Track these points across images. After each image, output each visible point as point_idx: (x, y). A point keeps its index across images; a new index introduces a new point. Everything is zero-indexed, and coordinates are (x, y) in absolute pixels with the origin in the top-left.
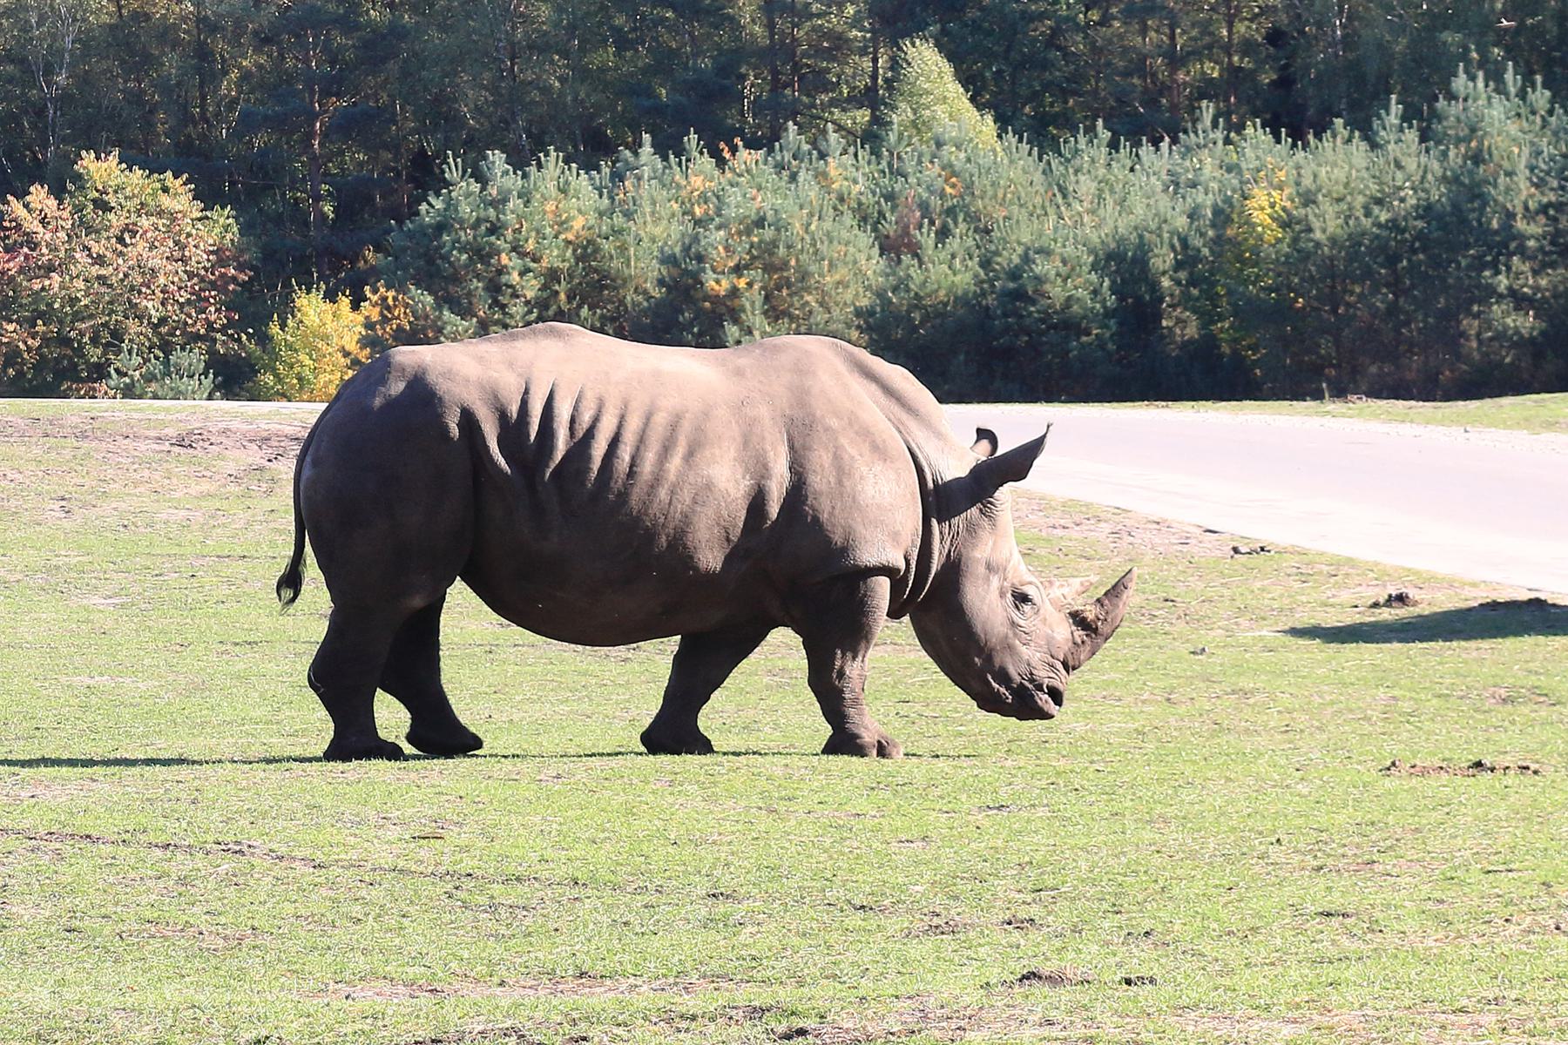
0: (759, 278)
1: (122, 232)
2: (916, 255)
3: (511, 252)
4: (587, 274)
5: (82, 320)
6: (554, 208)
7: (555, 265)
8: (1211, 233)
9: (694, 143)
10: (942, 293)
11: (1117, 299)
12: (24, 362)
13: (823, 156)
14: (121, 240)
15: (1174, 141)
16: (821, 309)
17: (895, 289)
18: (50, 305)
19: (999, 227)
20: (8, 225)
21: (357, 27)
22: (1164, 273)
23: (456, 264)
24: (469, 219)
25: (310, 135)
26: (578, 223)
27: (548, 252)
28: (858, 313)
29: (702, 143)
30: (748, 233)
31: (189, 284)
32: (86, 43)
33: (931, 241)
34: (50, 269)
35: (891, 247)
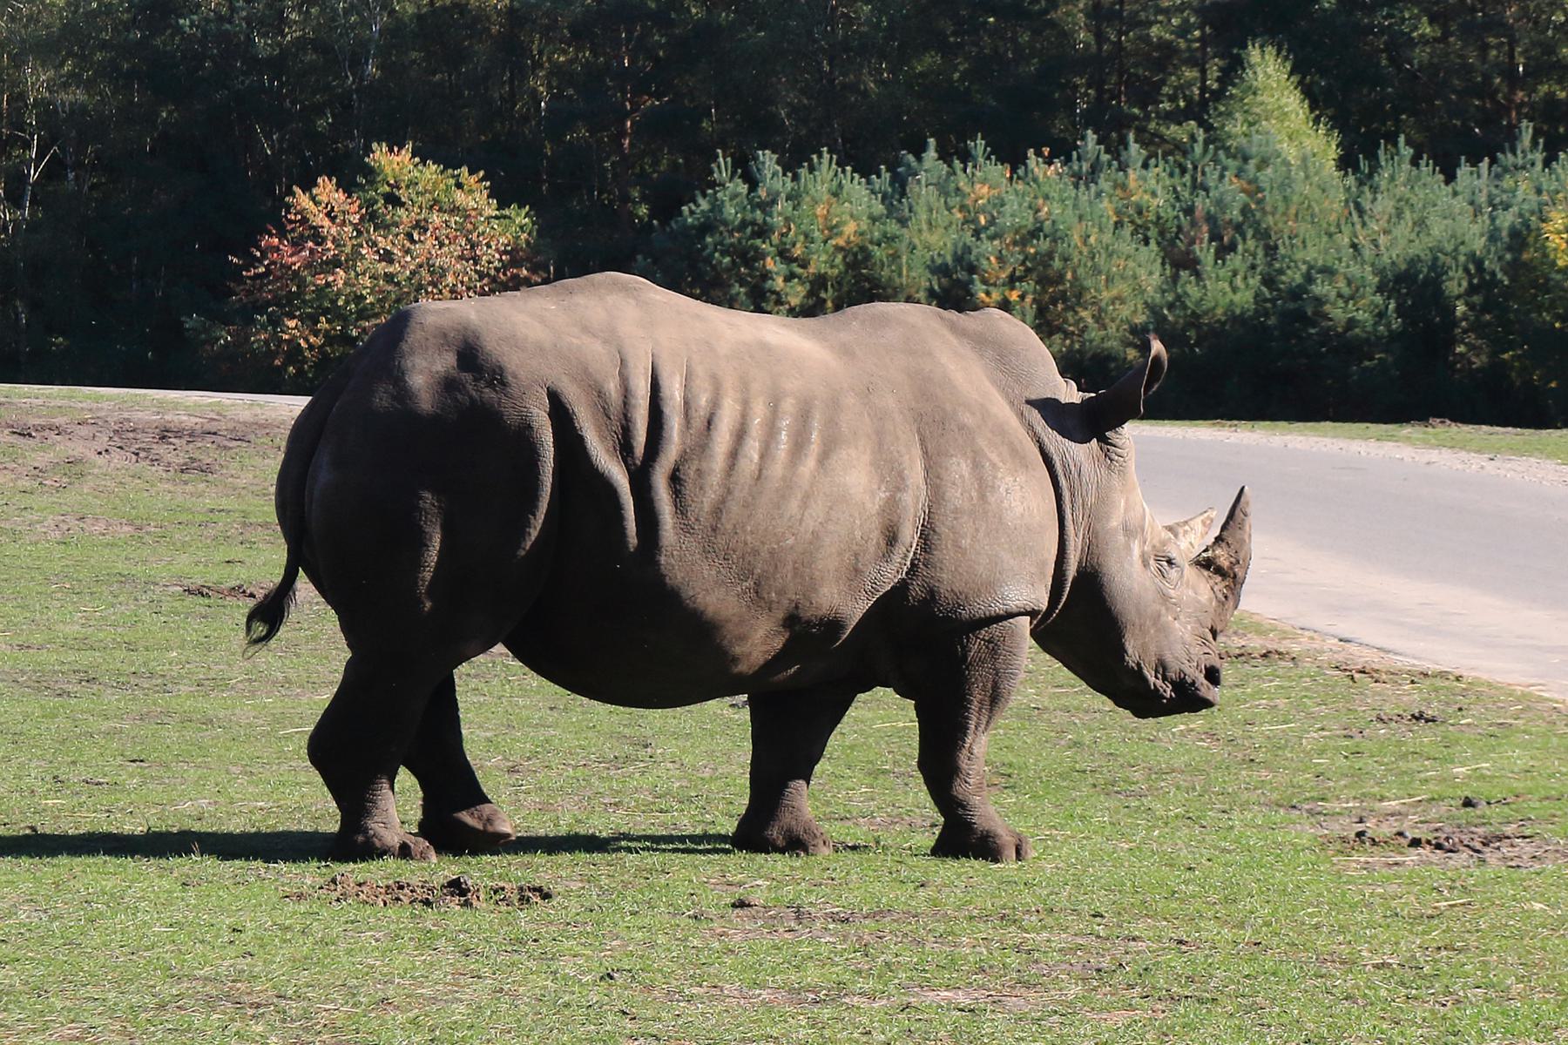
2: (1198, 275)
5: (367, 319)
6: (825, 212)
8: (1508, 257)
9: (980, 150)
10: (1219, 311)
11: (1403, 322)
12: (305, 360)
13: (1123, 168)
14: (410, 236)
15: (1493, 161)
16: (1096, 325)
17: (1171, 307)
18: (334, 302)
20: (293, 217)
22: (1458, 297)
23: (719, 268)
24: (733, 222)
25: (622, 133)
26: (850, 229)
29: (989, 149)
32: (396, 31)
33: (1210, 258)
34: (335, 263)
35: (1180, 262)
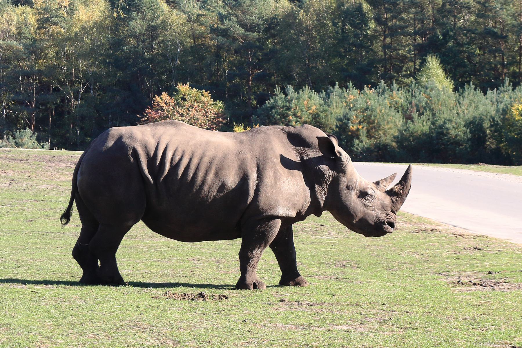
0: (366, 125)
1: (189, 107)
2: (413, 121)
3: (293, 115)
4: (316, 123)
6: (307, 103)
7: (306, 120)
9: (351, 86)
10: (419, 132)
13: (392, 91)
14: (188, 109)
17: (405, 130)
19: (437, 113)
20: (155, 104)
21: (263, 49)
25: (249, 80)
26: (314, 108)
27: (304, 116)
28: (394, 137)
30: (363, 112)
31: (208, 123)
32: (185, 51)
35: (408, 118)
